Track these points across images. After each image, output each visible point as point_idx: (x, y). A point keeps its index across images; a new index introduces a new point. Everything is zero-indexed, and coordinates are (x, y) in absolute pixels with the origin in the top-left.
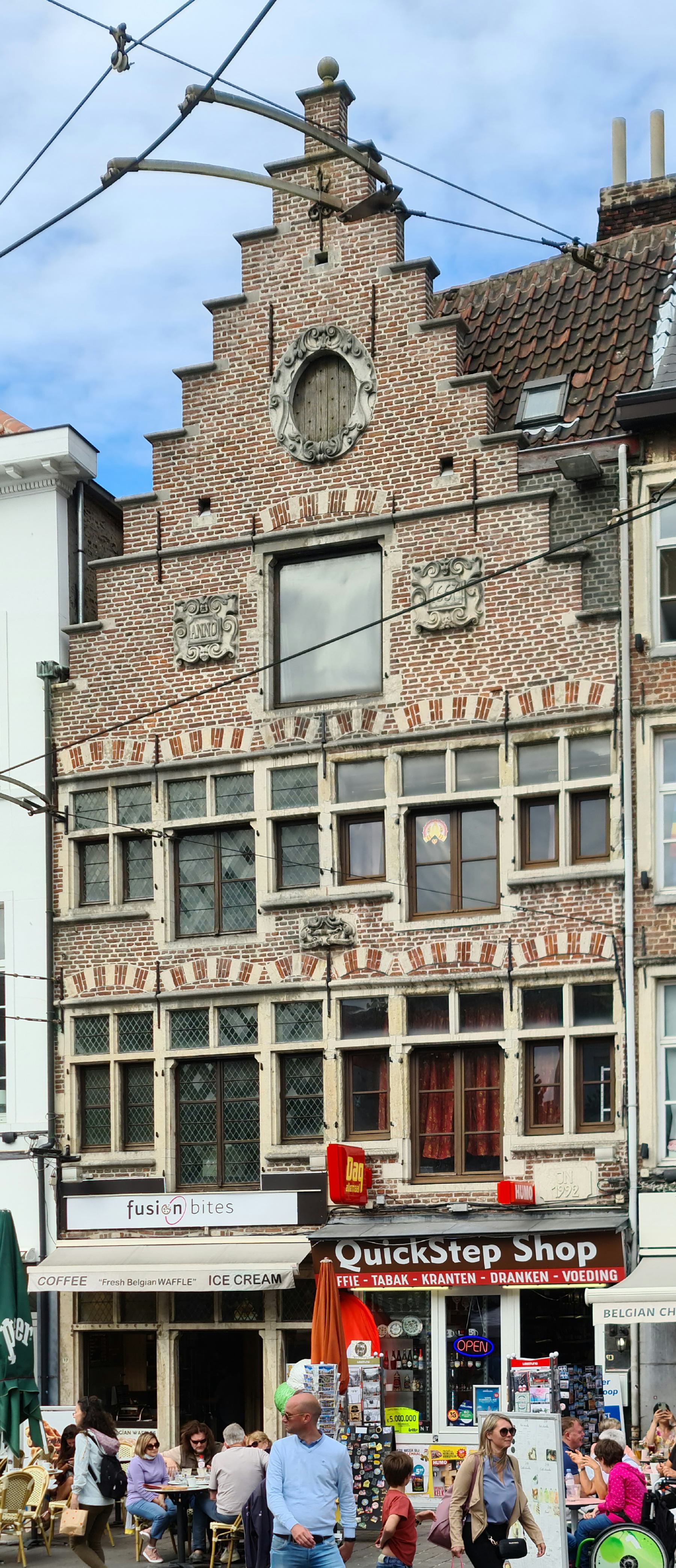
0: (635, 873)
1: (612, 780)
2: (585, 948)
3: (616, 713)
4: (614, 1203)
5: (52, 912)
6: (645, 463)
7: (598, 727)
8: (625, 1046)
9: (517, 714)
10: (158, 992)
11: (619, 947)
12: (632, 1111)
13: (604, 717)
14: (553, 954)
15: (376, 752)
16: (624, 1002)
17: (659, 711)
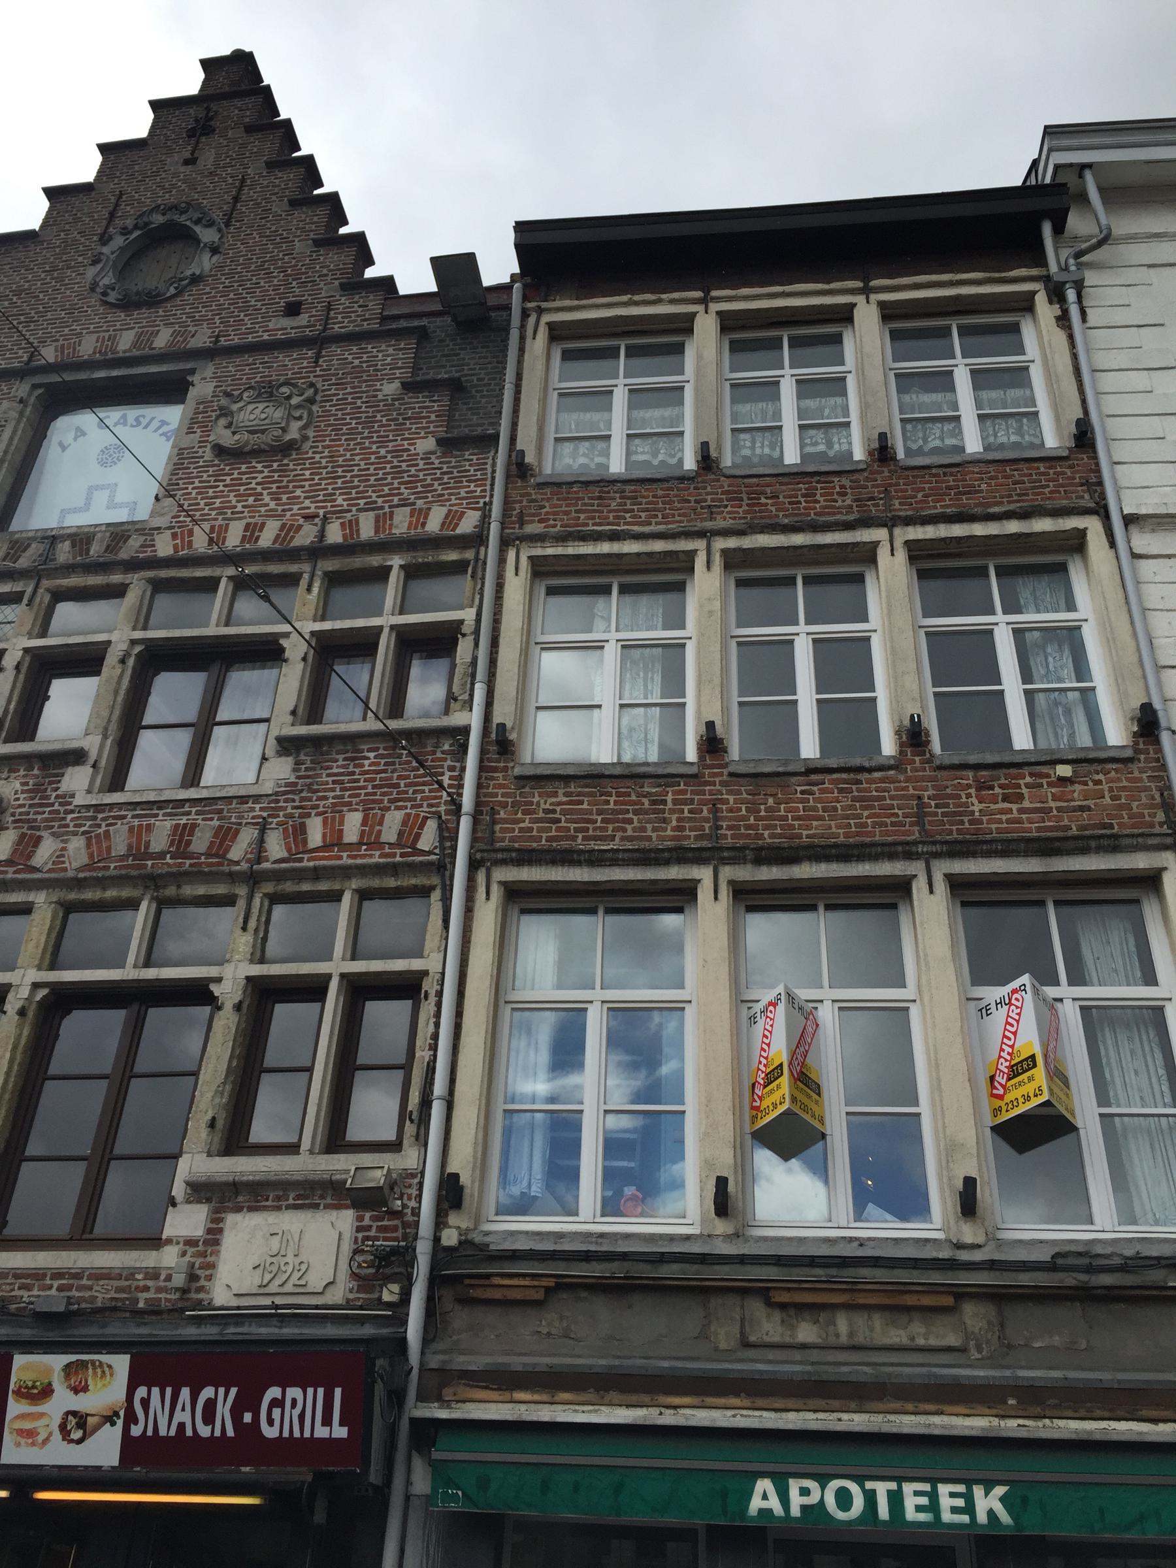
3: (478, 539)
5: (264, 754)
8: (440, 994)
10: (1130, 520)
11: (448, 835)
15: (116, 578)
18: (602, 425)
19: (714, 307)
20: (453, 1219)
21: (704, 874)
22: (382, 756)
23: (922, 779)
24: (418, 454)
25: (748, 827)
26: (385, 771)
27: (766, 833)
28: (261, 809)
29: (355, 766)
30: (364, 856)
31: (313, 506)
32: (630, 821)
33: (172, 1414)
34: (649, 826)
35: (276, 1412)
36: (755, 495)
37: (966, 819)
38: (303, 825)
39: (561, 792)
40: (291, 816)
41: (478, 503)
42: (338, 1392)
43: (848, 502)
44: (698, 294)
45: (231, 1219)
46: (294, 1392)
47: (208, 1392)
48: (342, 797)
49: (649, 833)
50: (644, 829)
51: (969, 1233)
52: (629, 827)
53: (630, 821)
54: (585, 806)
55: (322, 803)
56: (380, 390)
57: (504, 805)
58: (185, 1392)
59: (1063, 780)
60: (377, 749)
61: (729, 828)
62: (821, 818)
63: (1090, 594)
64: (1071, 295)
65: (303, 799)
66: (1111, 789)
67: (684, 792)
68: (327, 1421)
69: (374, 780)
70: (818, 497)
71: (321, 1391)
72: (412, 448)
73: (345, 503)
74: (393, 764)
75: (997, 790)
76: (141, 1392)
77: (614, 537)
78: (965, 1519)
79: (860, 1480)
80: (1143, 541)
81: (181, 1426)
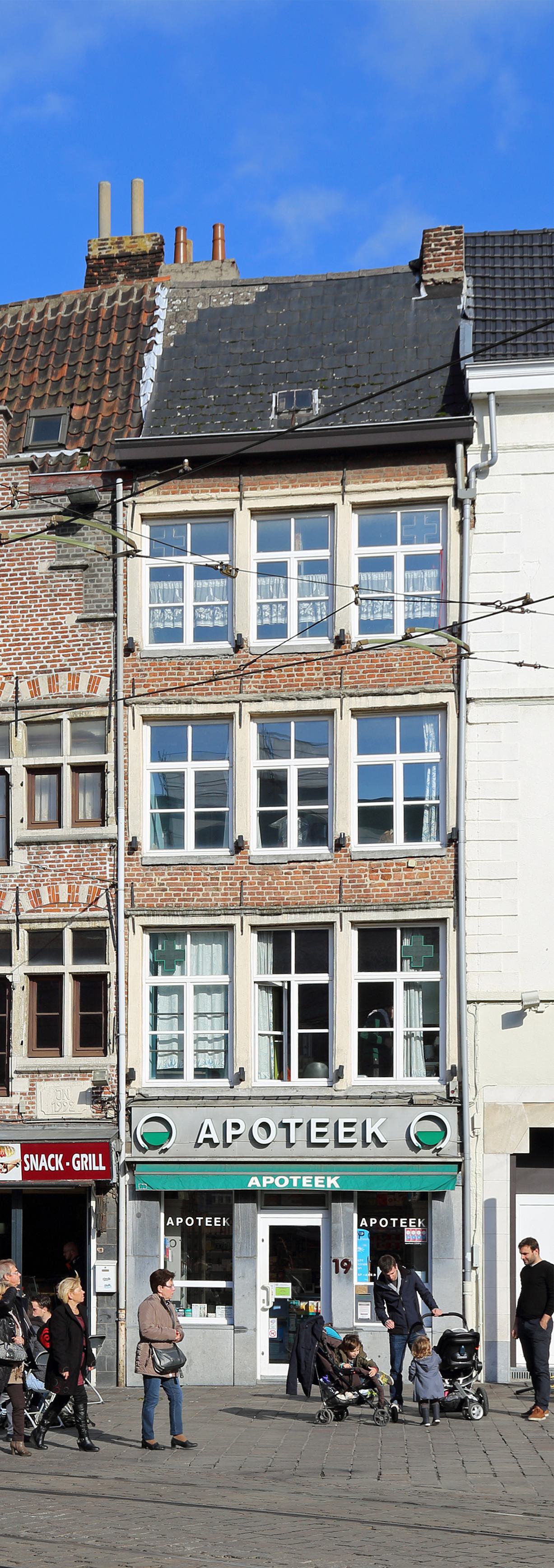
2: (83, 899)
8: (117, 983)
9: (26, 697)
10: (469, 701)
14: (55, 902)
16: (116, 947)
21: (234, 920)
22: (74, 851)
23: (343, 866)
24: (66, 628)
25: (259, 893)
26: (76, 861)
27: (267, 897)
28: (15, 881)
29: (60, 857)
30: (71, 910)
31: (9, 667)
32: (201, 890)
33: (37, 1163)
34: (210, 893)
35: (78, 1162)
37: (362, 889)
38: (38, 891)
39: (166, 873)
40: (30, 885)
41: (107, 670)
42: (100, 1155)
43: (321, 676)
45: (38, 1084)
46: (84, 1156)
47: (51, 1156)
48: (56, 875)
49: (210, 897)
50: (207, 894)
52: (201, 893)
53: (201, 890)
54: (179, 881)
55: (46, 878)
56: (36, 568)
57: (138, 881)
58: (43, 1156)
60: (70, 847)
61: (250, 894)
62: (294, 888)
64: (468, 508)
65: (35, 876)
66: (432, 873)
67: (227, 873)
68: (97, 1164)
69: (71, 865)
70: (304, 672)
71: (94, 1155)
72: (63, 621)
73: (28, 666)
74: (79, 856)
75: (380, 873)
76: (26, 1156)
78: (323, 1186)
79: (288, 1176)
81: (43, 1167)
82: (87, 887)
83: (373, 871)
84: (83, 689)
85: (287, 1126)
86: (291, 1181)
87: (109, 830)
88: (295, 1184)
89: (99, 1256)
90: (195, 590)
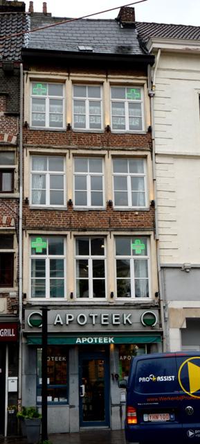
0: (23, 198)
1: (16, 167)
2: (4, 222)
3: (17, 146)
4: (13, 314)
6: (28, 70)
7: (11, 149)
8: (18, 257)
10: (156, 154)
11: (17, 222)
12: (20, 280)
13: (12, 146)
16: (18, 242)
17: (32, 147)
18: (43, 109)
19: (71, 78)
20: (25, 299)
21: (68, 233)
36: (80, 138)
44: (67, 74)
46: (5, 330)
51: (111, 300)
59: (136, 215)
63: (146, 170)
64: (16, 176)
77: (48, 148)
79: (92, 337)
80: (158, 159)
82: (6, 217)
83: (122, 216)
84: (5, 139)
85: (92, 317)
86: (94, 340)
87: (15, 195)
88: (96, 341)
89: (9, 376)
90: (50, 108)
